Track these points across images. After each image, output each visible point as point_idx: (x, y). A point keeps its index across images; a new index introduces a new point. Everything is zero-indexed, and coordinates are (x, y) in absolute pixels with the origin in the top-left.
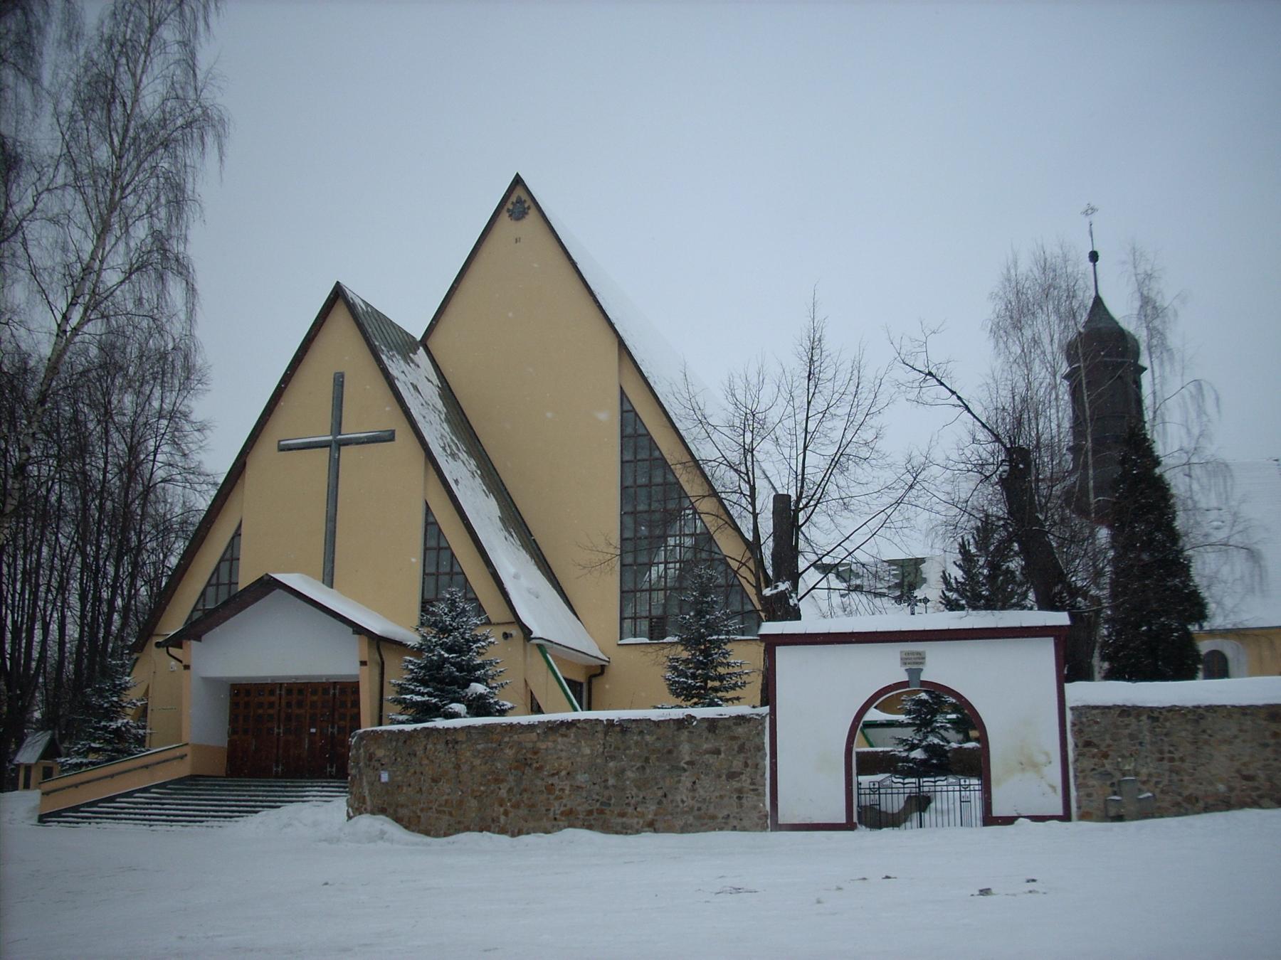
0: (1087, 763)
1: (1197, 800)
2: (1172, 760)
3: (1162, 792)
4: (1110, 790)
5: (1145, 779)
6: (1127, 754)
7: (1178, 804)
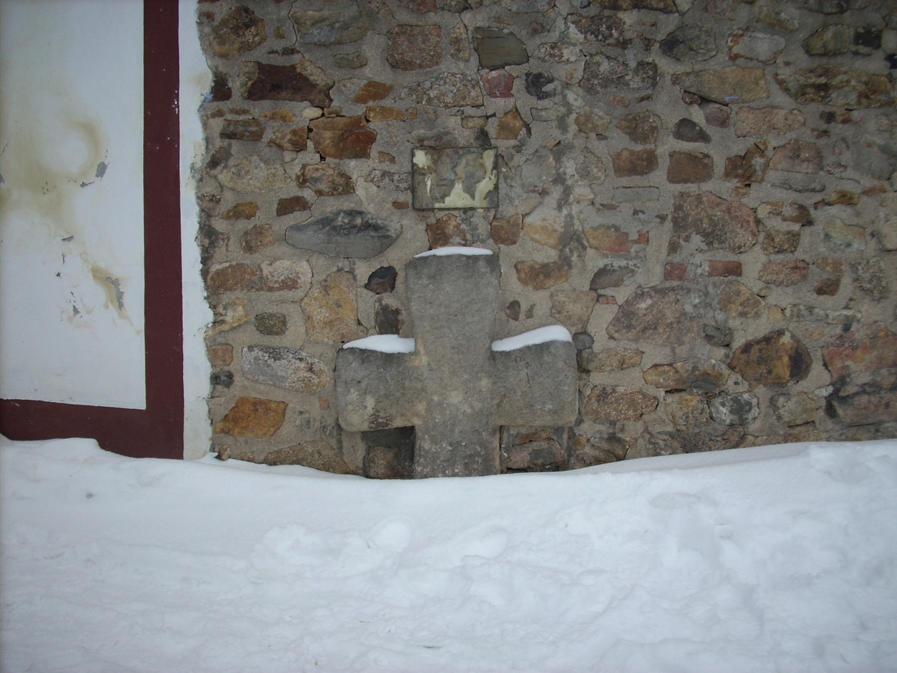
0: (264, 177)
1: (799, 364)
2: (691, 168)
3: (626, 318)
4: (367, 303)
5: (548, 255)
6: (464, 136)
7: (706, 385)
